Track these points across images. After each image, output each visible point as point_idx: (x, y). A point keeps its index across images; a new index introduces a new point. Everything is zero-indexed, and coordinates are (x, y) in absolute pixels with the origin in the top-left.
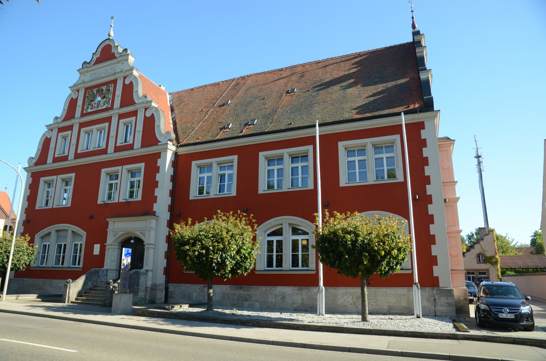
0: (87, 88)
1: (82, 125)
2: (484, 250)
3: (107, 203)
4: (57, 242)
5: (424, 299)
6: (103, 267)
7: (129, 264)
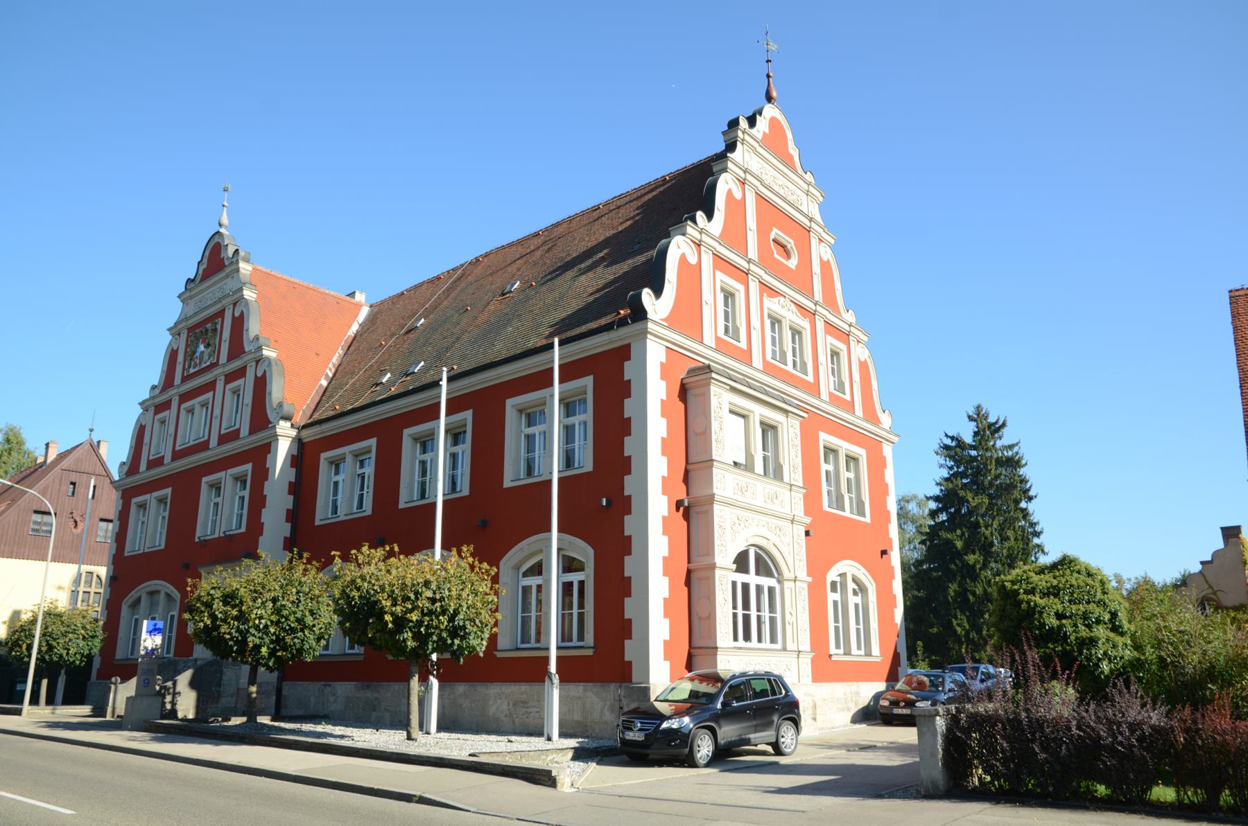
0: (191, 328)
1: (184, 398)
2: (1215, 589)
3: (205, 540)
4: (150, 615)
5: (606, 707)
6: (192, 656)
7: (158, 647)
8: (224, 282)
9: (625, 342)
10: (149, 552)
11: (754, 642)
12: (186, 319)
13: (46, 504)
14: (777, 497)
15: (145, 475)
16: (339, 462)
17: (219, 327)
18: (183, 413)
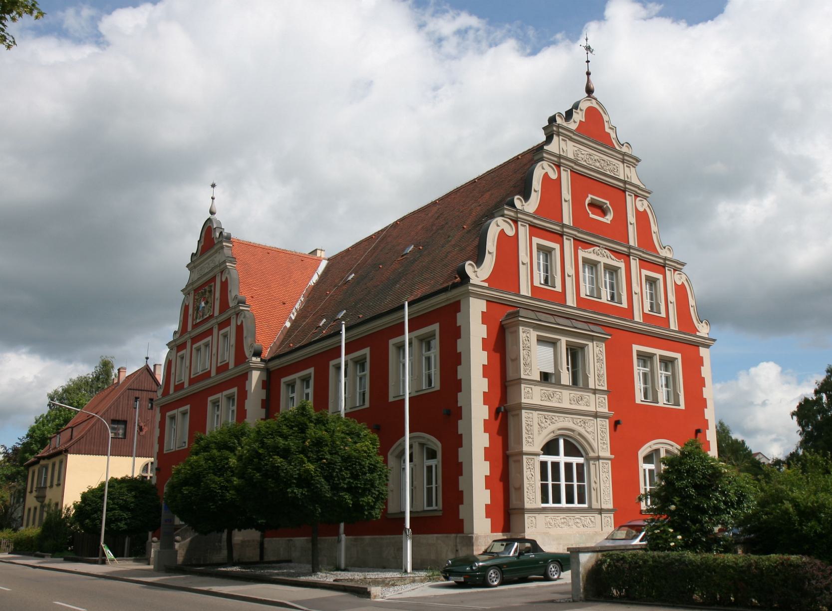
1: (195, 340)
8: (213, 257)
9: (457, 299)
10: (168, 453)
11: (564, 504)
12: (192, 284)
13: (104, 423)
14: (582, 399)
15: (234, 371)
16: (429, 339)
17: (213, 289)
18: (194, 351)
